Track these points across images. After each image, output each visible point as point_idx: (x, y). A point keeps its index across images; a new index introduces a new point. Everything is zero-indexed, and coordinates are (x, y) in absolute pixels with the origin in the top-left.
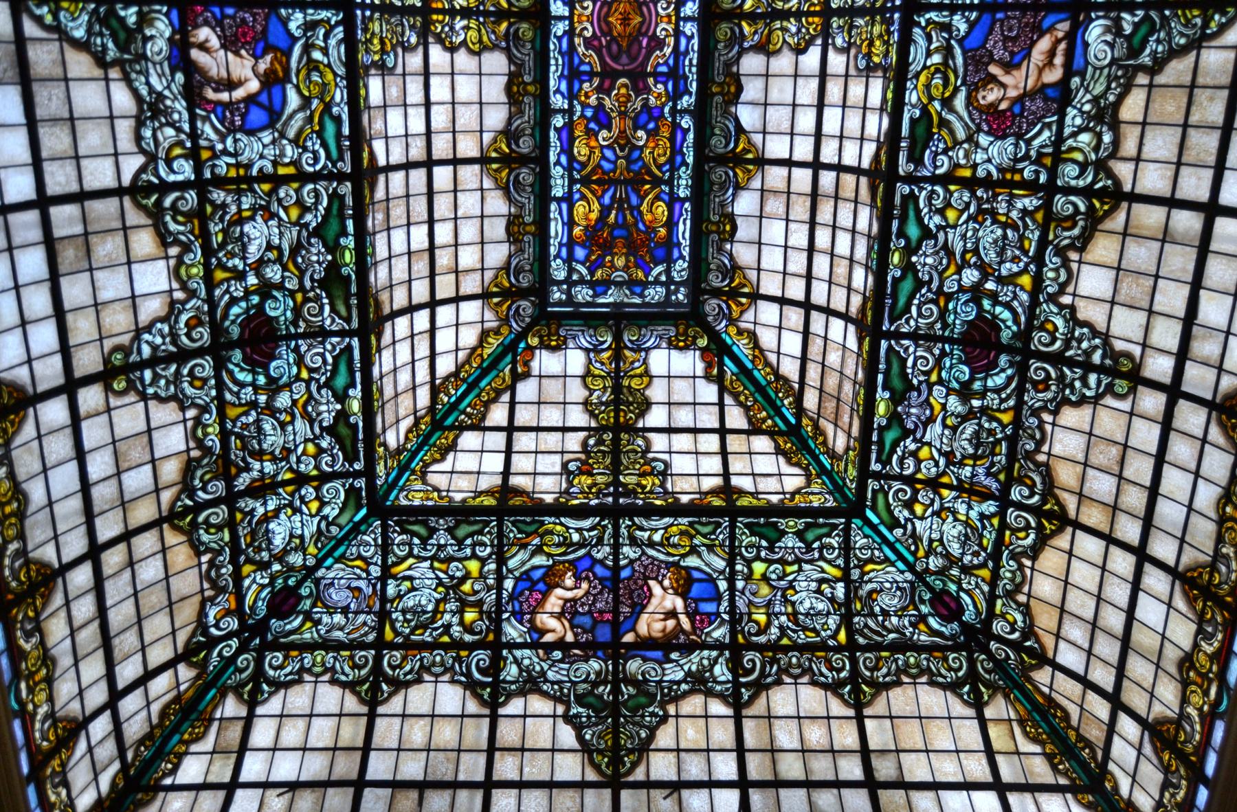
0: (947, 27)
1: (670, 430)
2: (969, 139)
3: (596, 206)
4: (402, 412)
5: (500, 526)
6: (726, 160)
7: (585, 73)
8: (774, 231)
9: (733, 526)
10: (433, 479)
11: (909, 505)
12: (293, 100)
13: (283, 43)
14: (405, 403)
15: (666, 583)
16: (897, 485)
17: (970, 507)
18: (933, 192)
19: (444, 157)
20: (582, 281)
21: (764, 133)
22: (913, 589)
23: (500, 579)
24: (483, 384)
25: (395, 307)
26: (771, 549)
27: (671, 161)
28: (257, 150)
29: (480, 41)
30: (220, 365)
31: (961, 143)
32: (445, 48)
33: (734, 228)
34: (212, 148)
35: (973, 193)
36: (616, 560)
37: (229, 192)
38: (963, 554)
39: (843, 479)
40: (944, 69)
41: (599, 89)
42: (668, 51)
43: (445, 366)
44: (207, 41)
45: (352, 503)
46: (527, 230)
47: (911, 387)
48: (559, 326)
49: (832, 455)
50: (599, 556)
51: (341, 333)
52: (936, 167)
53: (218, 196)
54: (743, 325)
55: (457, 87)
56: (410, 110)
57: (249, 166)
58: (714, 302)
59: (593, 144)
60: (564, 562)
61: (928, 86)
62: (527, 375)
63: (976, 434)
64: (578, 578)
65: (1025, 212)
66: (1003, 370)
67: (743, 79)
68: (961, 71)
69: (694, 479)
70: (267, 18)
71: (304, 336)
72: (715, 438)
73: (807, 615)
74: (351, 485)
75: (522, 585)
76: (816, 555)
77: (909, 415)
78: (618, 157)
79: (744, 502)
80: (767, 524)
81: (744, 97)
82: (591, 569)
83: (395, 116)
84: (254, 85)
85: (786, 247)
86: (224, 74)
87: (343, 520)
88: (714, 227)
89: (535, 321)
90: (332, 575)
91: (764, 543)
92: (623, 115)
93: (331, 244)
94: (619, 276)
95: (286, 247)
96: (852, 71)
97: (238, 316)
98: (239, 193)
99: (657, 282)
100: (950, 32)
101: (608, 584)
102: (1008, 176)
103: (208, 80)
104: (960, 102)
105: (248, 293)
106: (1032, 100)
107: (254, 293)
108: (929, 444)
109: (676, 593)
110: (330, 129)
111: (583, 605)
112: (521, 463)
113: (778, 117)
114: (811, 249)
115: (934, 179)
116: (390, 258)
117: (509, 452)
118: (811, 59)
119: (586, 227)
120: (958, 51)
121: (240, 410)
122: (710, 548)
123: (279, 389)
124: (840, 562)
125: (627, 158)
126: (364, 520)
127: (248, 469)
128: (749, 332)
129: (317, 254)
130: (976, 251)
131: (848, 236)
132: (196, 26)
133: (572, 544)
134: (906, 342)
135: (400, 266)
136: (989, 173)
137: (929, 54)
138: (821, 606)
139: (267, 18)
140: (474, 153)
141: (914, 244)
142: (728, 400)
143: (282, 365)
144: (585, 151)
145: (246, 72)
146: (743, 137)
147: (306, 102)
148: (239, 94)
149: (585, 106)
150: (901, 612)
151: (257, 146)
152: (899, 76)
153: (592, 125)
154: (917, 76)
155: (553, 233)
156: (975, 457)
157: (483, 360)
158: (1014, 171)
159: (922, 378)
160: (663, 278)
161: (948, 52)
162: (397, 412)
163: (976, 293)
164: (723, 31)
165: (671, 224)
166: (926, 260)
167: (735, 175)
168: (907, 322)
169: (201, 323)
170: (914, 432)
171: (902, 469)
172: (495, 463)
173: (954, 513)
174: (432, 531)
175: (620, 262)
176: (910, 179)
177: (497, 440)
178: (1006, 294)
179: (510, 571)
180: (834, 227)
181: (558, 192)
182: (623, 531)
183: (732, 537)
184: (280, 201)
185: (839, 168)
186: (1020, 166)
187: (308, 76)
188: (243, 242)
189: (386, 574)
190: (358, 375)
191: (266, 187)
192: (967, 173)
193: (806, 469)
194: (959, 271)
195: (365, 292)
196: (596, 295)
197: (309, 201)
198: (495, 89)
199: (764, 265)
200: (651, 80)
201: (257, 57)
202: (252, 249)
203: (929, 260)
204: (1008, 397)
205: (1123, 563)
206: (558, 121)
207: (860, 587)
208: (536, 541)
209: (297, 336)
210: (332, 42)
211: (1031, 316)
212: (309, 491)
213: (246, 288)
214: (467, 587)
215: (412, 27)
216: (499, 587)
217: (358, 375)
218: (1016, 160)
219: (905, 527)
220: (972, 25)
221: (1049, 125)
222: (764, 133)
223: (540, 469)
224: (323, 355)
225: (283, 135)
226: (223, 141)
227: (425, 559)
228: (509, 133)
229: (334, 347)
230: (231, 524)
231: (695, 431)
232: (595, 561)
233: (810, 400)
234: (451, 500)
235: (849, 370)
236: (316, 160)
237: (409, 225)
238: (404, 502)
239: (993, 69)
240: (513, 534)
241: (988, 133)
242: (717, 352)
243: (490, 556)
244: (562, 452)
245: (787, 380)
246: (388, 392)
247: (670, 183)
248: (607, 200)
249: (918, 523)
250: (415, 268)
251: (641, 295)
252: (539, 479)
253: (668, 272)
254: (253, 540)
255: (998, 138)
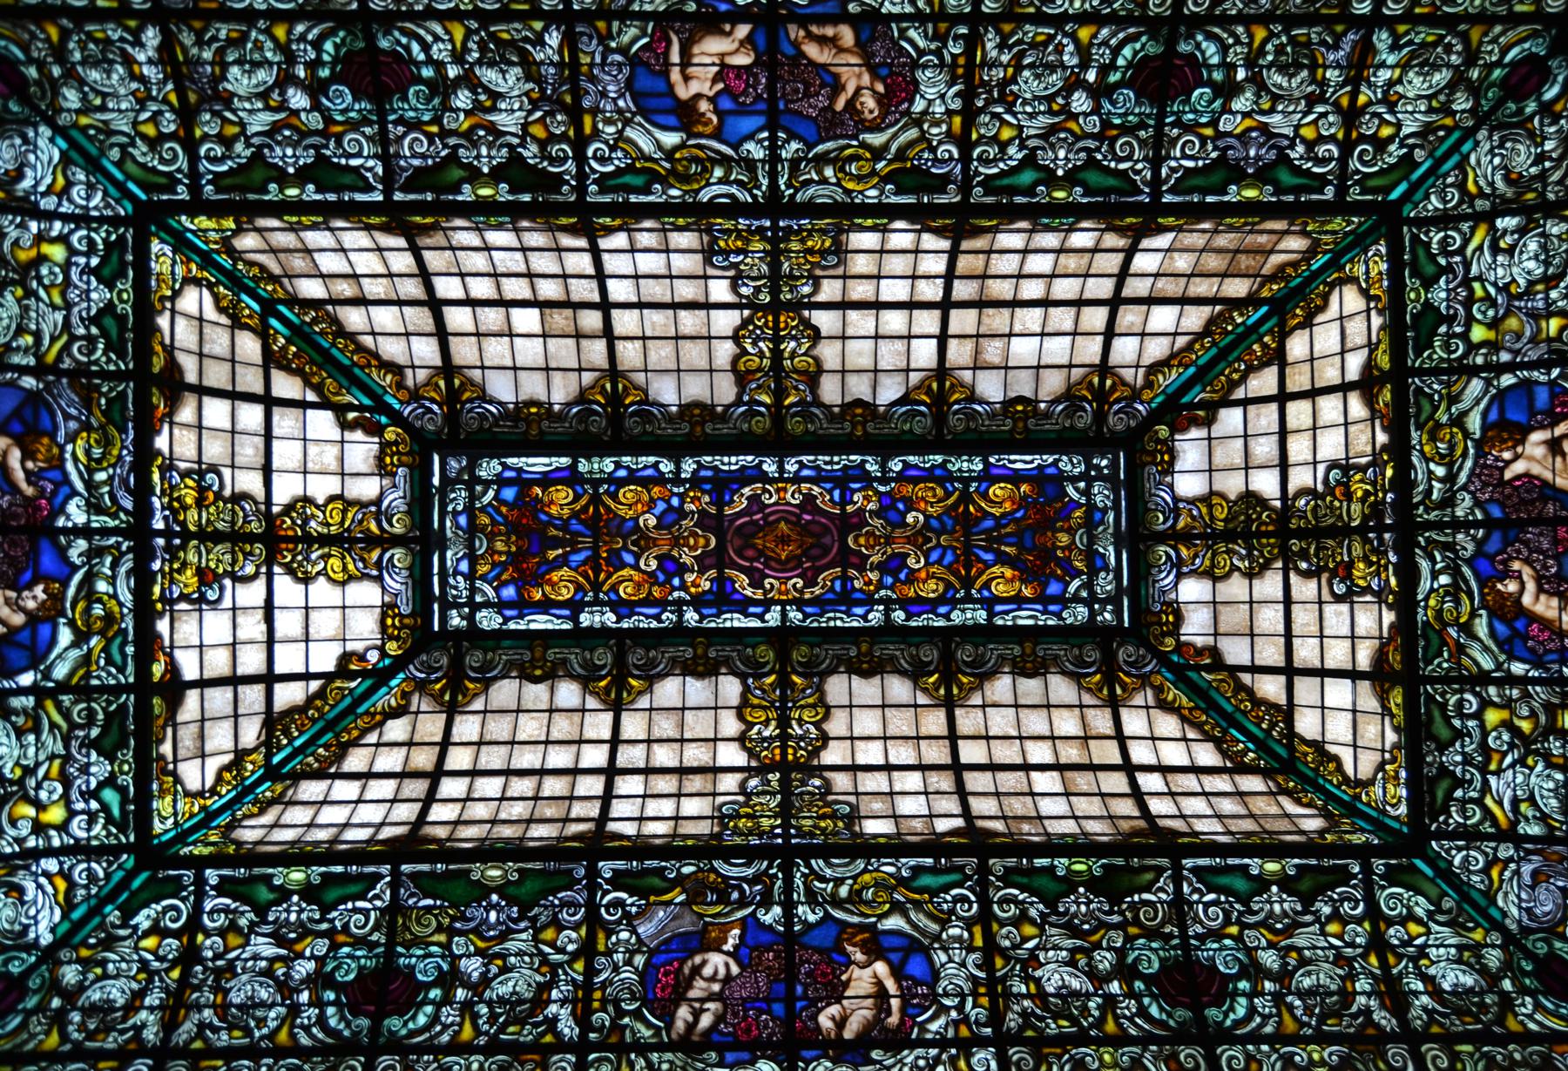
0: (795, 163)
1: (1284, 465)
2: (918, 123)
3: (997, 570)
4: (1274, 810)
5: (1432, 680)
6: (942, 413)
7: (843, 586)
8: (1024, 350)
9: (1421, 372)
10: (1365, 771)
11: (1380, 145)
12: (894, 922)
13: (833, 931)
14: (1262, 805)
15: (1507, 455)
16: (1354, 164)
17: (1383, 65)
18: (979, 159)
19: (947, 750)
20: (1089, 585)
21: (908, 370)
22: (1501, 126)
23: (1512, 680)
24: (1229, 709)
25: (1136, 813)
26: (1450, 320)
27: (941, 482)
28: (955, 969)
29: (814, 706)
30: (1228, 1036)
31: (923, 132)
32: (824, 746)
33: (1020, 399)
34: (956, 1023)
35: (982, 110)
36: (1476, 524)
37: (1008, 1008)
38: (1448, 66)
39: (1347, 234)
40: (840, 163)
41: (861, 569)
42: (816, 490)
43: (1207, 755)
44: (833, 1018)
45: (1406, 878)
46: (1031, 654)
47: (1223, 158)
48: (1149, 611)
49: (1310, 253)
50: (1470, 547)
51: (1177, 880)
52: (951, 158)
53: (1012, 1021)
54: (1140, 381)
55: (867, 733)
56: (897, 788)
57: (974, 979)
58: (1111, 420)
59: (923, 575)
60: (1482, 594)
61: (859, 179)
62: (1214, 651)
63: (1283, 69)
64: (1506, 575)
65: (1001, 47)
66: (1198, 45)
67: (848, 399)
68: (842, 142)
69: (1352, 429)
70: (805, 947)
71: (1183, 928)
72: (1292, 407)
73: (1547, 263)
74: (1382, 877)
75: (1519, 649)
76: (1457, 259)
77: (1258, 158)
78: (938, 545)
79: (1384, 361)
80: (1414, 327)
81: (868, 398)
82: (1491, 558)
83: (907, 806)
84: (881, 968)
85: (1042, 334)
86: (869, 1002)
87: (1433, 892)
88: (1020, 424)
89: (1143, 642)
90: (1515, 911)
91: (1443, 329)
92: (889, 540)
93: (1064, 887)
94: (1080, 539)
95: (1069, 943)
96: (840, 271)
97: (1161, 1009)
98: (1008, 995)
99: (1087, 493)
100: (800, 160)
101: (1512, 534)
102: (960, 71)
103: (877, 1021)
104: (876, 139)
105: (1131, 994)
106: (874, 55)
107: (1131, 987)
108: (1297, 127)
109: (1523, 442)
110: (927, 880)
111: (1546, 567)
112: (1337, 655)
113: (890, 354)
114: (1045, 303)
115: (965, 159)
116: (1075, 818)
117: (1322, 673)
118: (825, 321)
119: (1023, 581)
120: (820, 148)
121: (1286, 1016)
122: (1454, 399)
123: (1255, 963)
124: (1465, 227)
125: (939, 534)
126: (1431, 862)
127: (1367, 1012)
128: (1147, 375)
129: (1078, 905)
130: (1050, 99)
131: (1031, 258)
132: (818, 1028)
133: (1455, 584)
134: (1164, 171)
135: (1084, 806)
136: (957, 95)
137: (824, 181)
138: (1533, 246)
139: (805, 947)
140: (941, 714)
141: (1042, 175)
142: (1239, 394)
143: (1223, 958)
144: (932, 585)
145: (868, 975)
146: (914, 396)
147: (897, 908)
148: (891, 986)
149: (880, 585)
150: (1536, 138)
151: (951, 969)
152: (848, 214)
153: (902, 576)
154: (848, 192)
155: (1031, 622)
156: (1313, 67)
157: (1197, 707)
158: (954, 65)
159: (1210, 147)
160: (1082, 485)
161: (821, 160)
162: (1274, 816)
163: (1100, 92)
164: (795, 426)
165: (1015, 478)
166: (1061, 158)
167: (957, 402)
168: (1138, 172)
169: (1175, 1056)
170: (1281, 150)
171: (1331, 159)
172: (1339, 692)
173: (1391, 83)
174: (1444, 771)
175: (1064, 539)
176: (965, 188)
177: (1305, 689)
178: (1101, 55)
179: (1499, 666)
180: (1020, 276)
181: (981, 615)
182: (1433, 516)
183: (1435, 372)
184: (1015, 947)
185: (949, 276)
186: (948, 58)
187: (867, 903)
188: (1067, 995)
189: (1509, 835)
190: (1230, 861)
191: (999, 962)
192: (957, 120)
193: (1332, 286)
194: (1075, 117)
195: (1123, 846)
196: (1106, 568)
197: (1013, 910)
198: (866, 689)
199: (1065, 361)
200: (850, 509)
201: (849, 962)
202: (1075, 984)
203: (1062, 154)
204: (1233, 34)
205: (424, 759)
206: (899, 616)
207: (1502, 196)
208: (1453, 632)
209: (1184, 936)
210: (828, 872)
211: (1129, 20)
212: (1394, 934)
213: (1125, 996)
214: (1526, 726)
215: (804, 783)
216: (1523, 681)
217: (1230, 861)
218: (942, 65)
219: (1412, 147)
220: (792, 136)
221: (902, 31)
222: (908, 370)
223: (1346, 631)
224: (1207, 905)
225: (937, 938)
226: (948, 1009)
227: (1486, 783)
228: (915, 675)
229: (1195, 890)
230: (1448, 1041)
231: (1283, 433)
232: (1479, 552)
233: (1237, 288)
234: (1396, 746)
235: (1198, 240)
236: (963, 899)
237: (1032, 794)
238: (1403, 810)
239: (840, 105)
240: (1443, 663)
241: (912, 102)
242: (1182, 412)
243: (1476, 694)
244: (1320, 603)
245: (1211, 321)
246: (1248, 825)
247: (966, 482)
248: (988, 557)
249: (1406, 131)
250: (1085, 788)
251: (1104, 511)
252: (1360, 631)
253: (1074, 480)
254: (1469, 1013)
255: (917, 90)
